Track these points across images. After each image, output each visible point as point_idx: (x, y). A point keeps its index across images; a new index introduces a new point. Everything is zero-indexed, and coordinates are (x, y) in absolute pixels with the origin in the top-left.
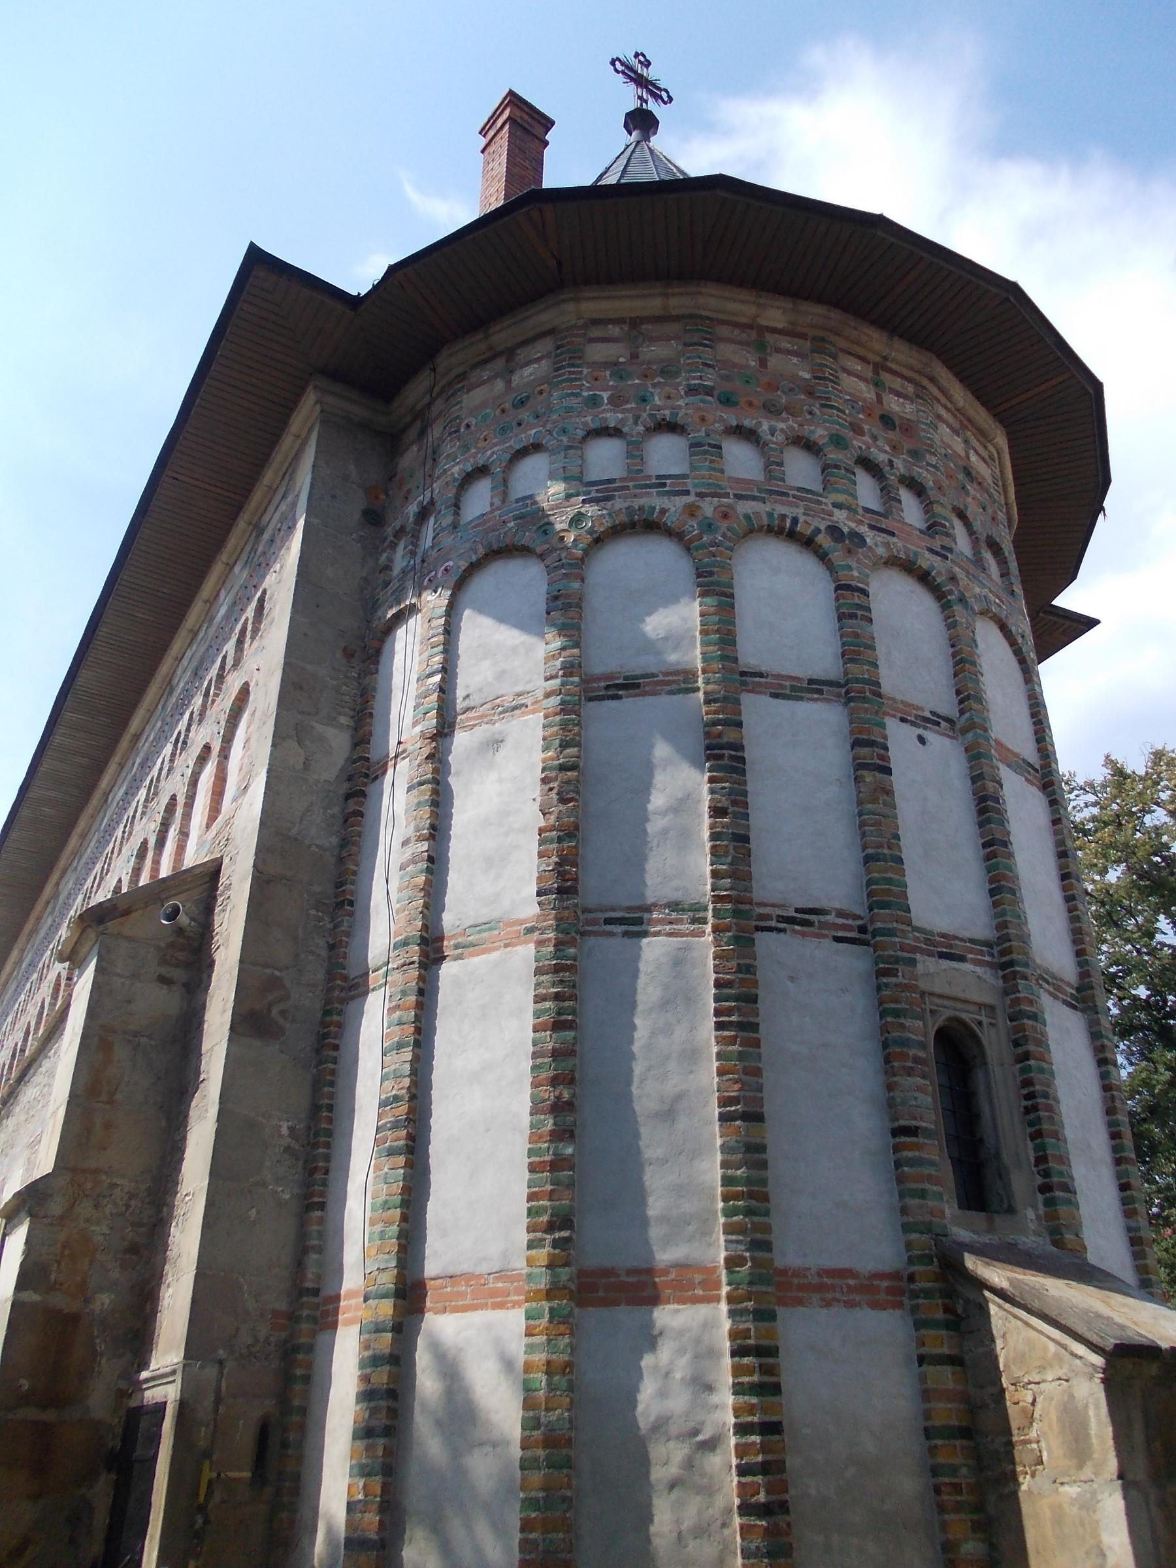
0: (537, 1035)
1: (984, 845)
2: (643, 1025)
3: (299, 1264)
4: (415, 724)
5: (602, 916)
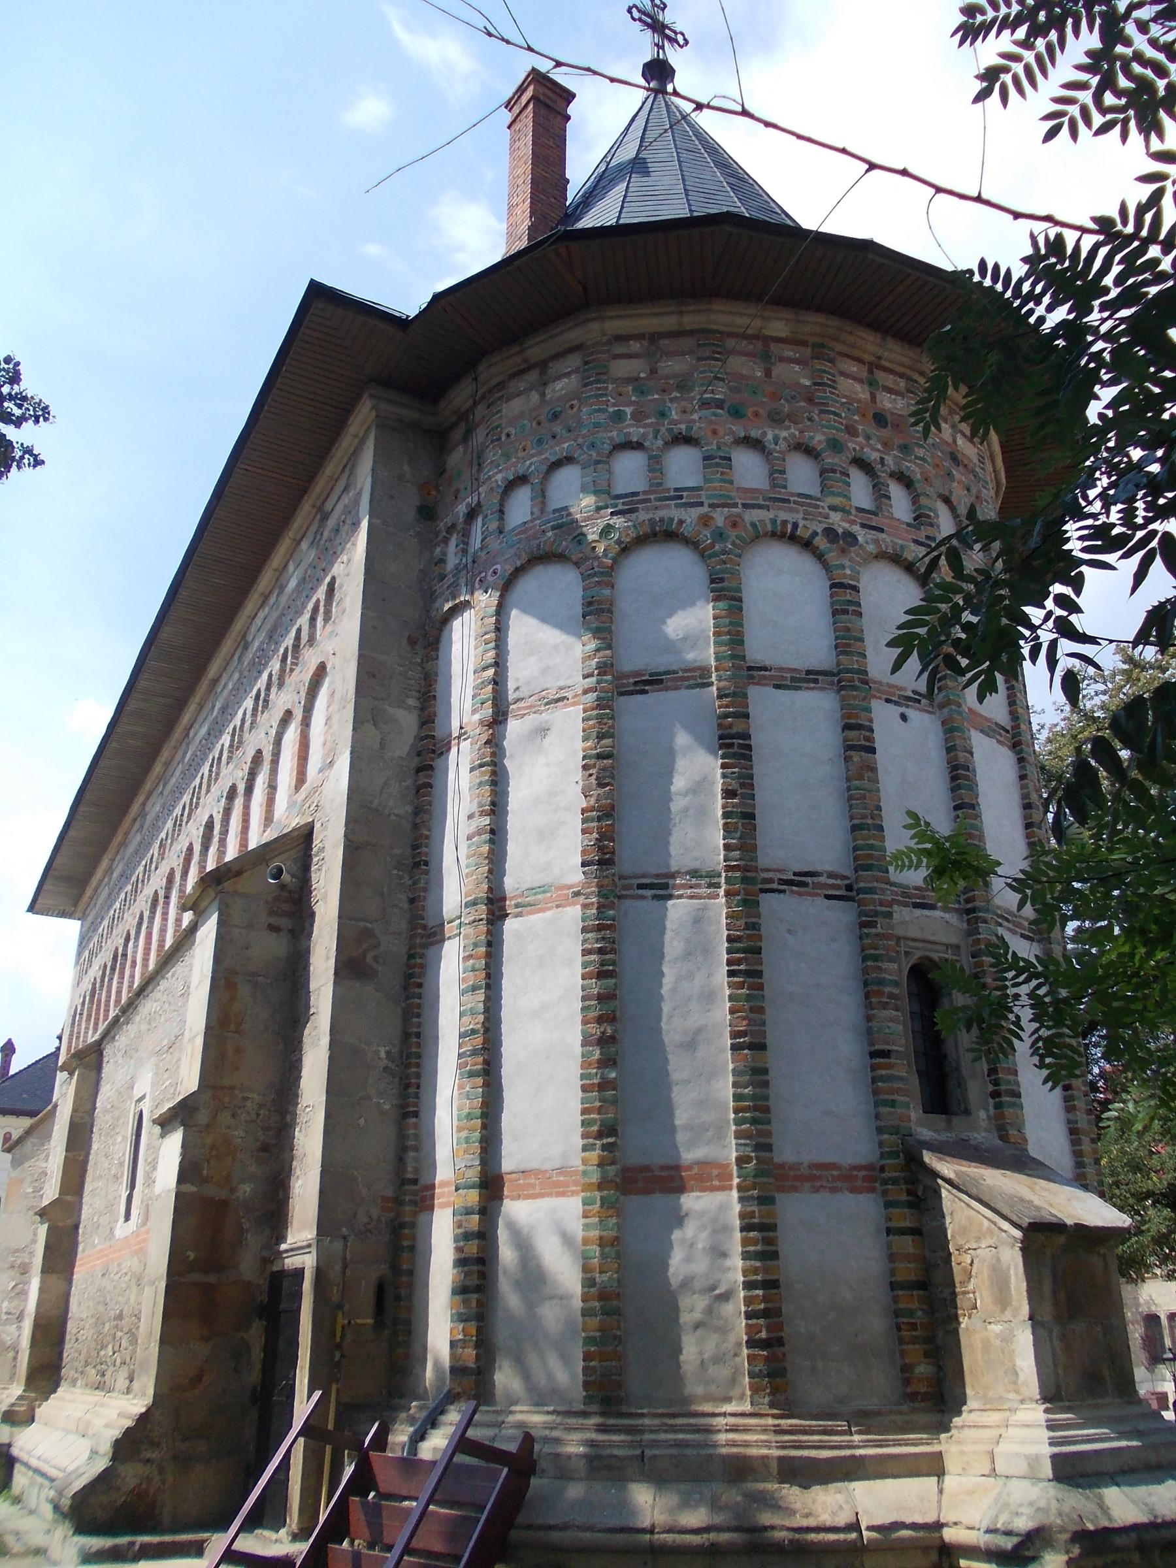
0: (585, 982)
1: (956, 808)
2: (670, 974)
3: (401, 1160)
4: (474, 712)
5: (636, 882)
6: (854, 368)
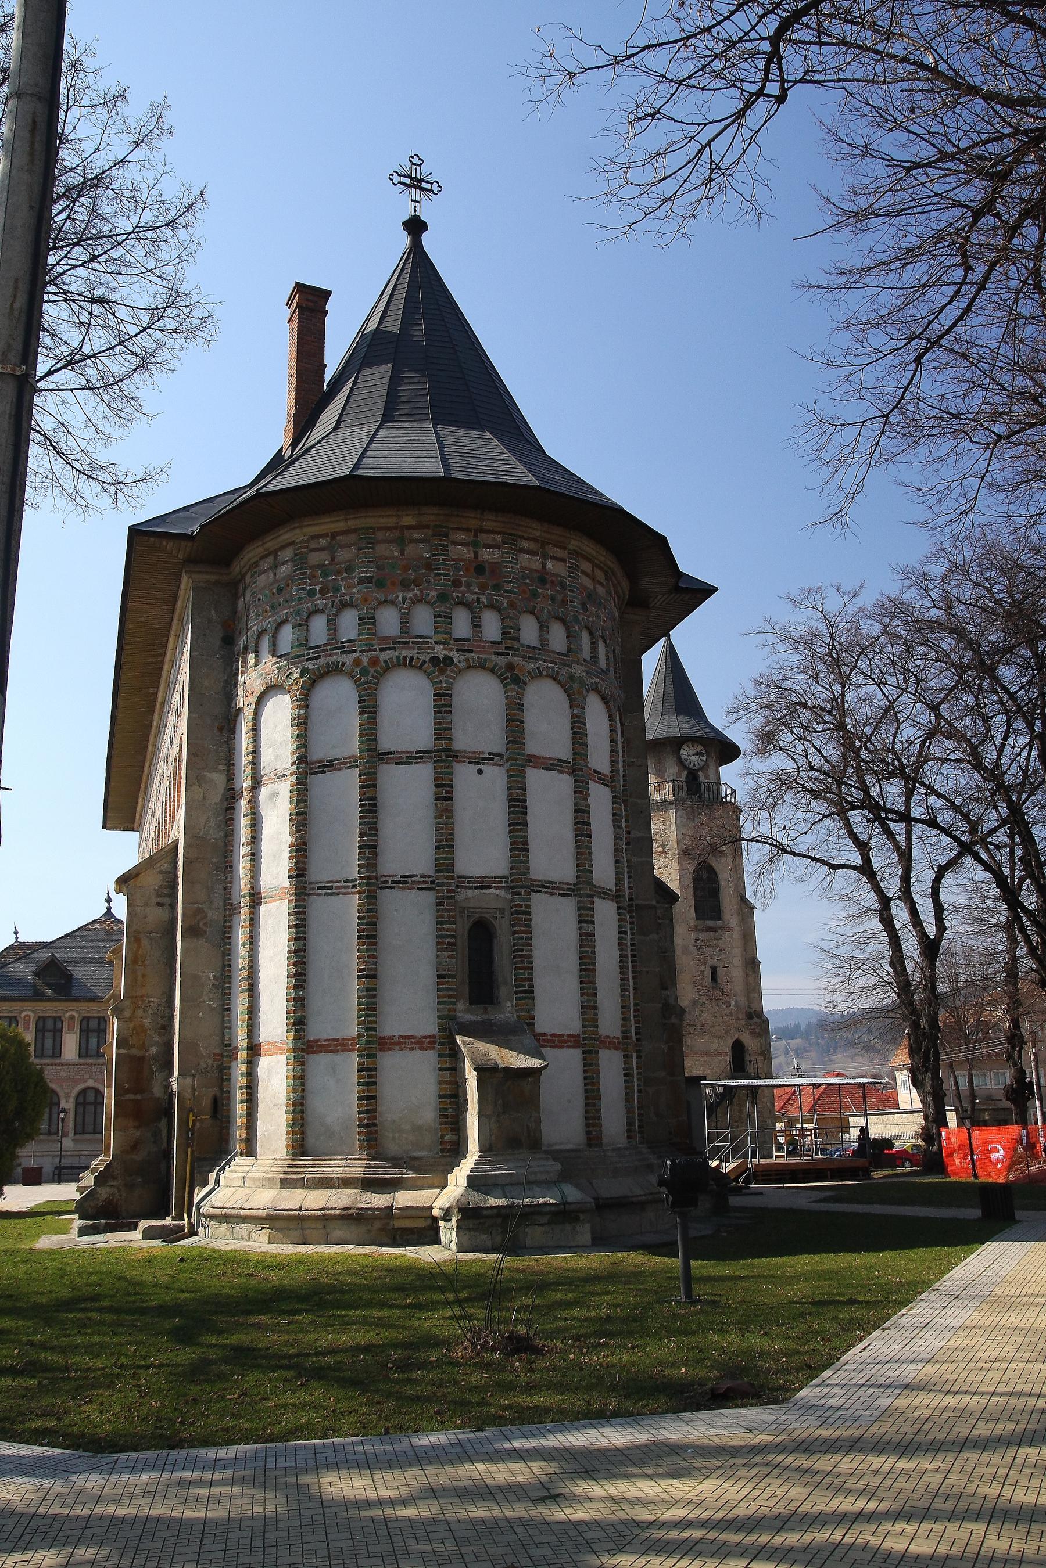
6: (462, 537)
